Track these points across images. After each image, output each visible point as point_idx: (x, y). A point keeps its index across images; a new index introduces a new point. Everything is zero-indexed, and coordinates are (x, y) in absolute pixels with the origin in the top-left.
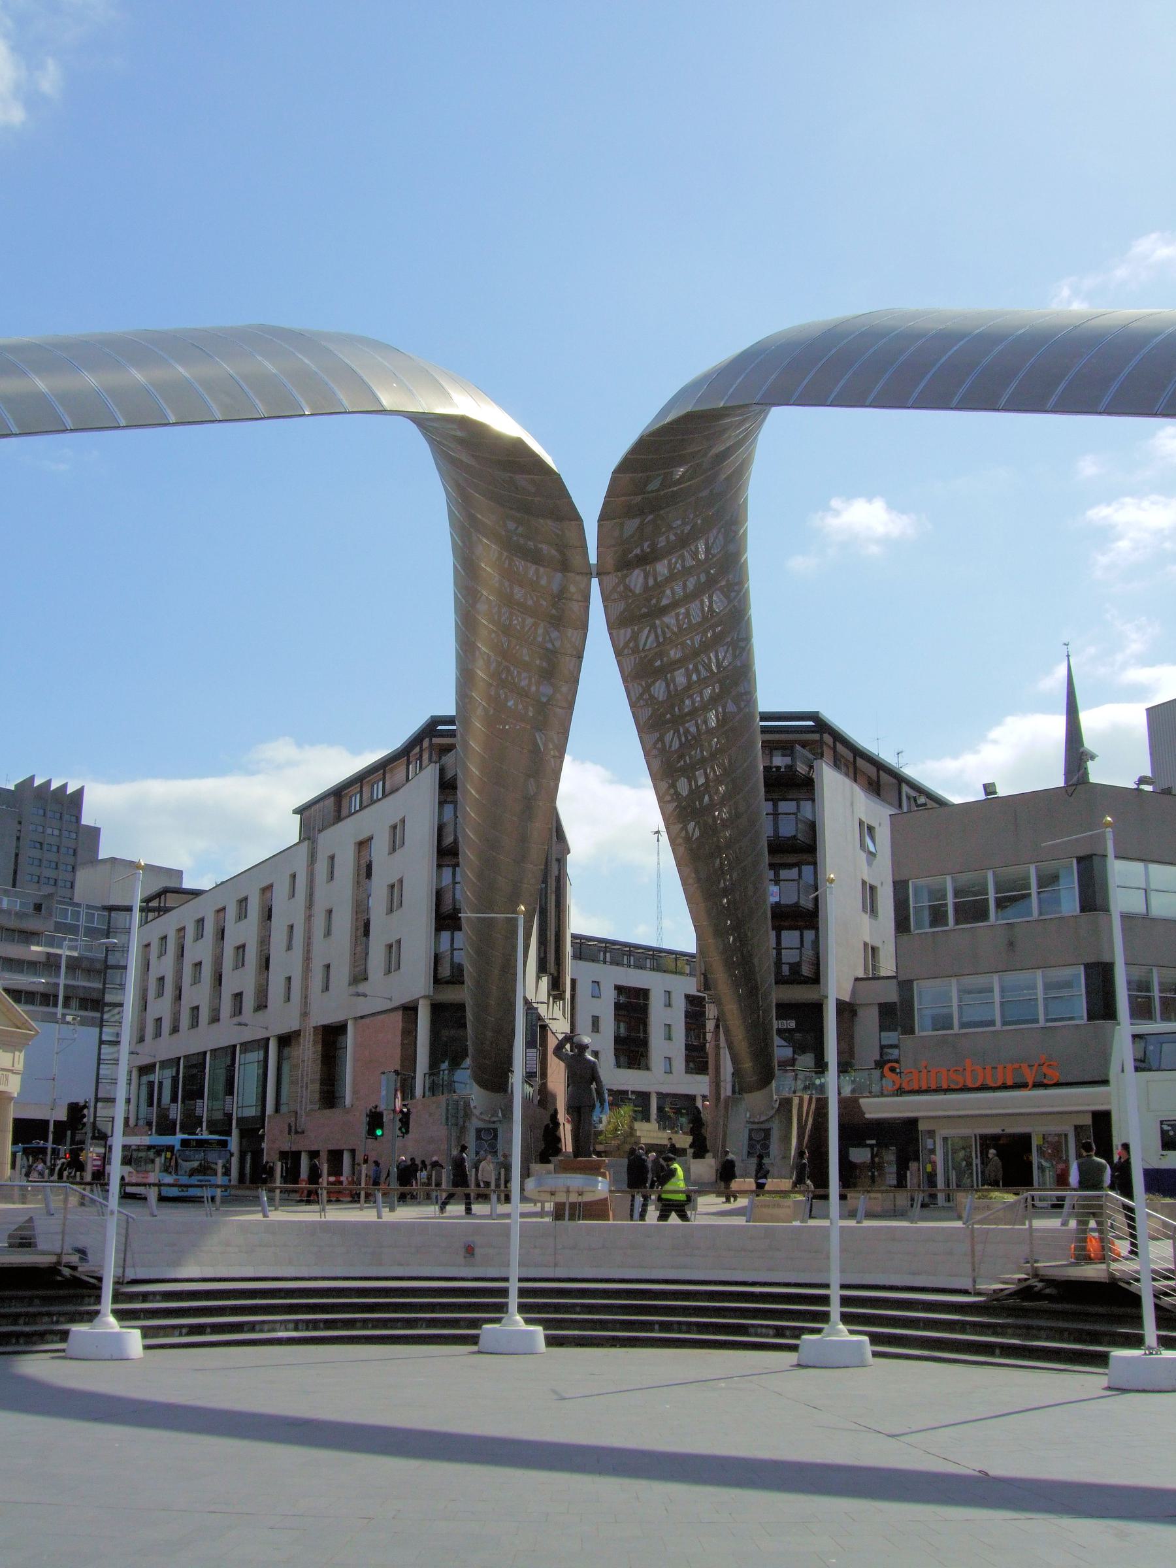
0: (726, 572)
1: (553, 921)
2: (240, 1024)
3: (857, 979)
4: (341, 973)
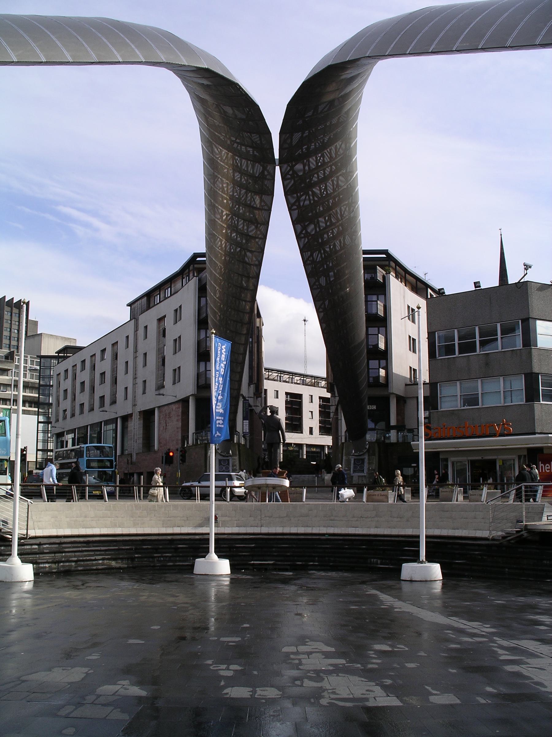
0: (343, 164)
1: (256, 356)
2: (103, 411)
3: (406, 385)
4: (151, 385)
